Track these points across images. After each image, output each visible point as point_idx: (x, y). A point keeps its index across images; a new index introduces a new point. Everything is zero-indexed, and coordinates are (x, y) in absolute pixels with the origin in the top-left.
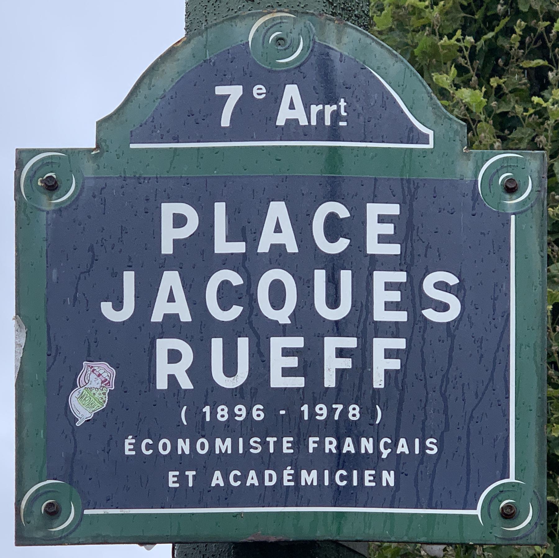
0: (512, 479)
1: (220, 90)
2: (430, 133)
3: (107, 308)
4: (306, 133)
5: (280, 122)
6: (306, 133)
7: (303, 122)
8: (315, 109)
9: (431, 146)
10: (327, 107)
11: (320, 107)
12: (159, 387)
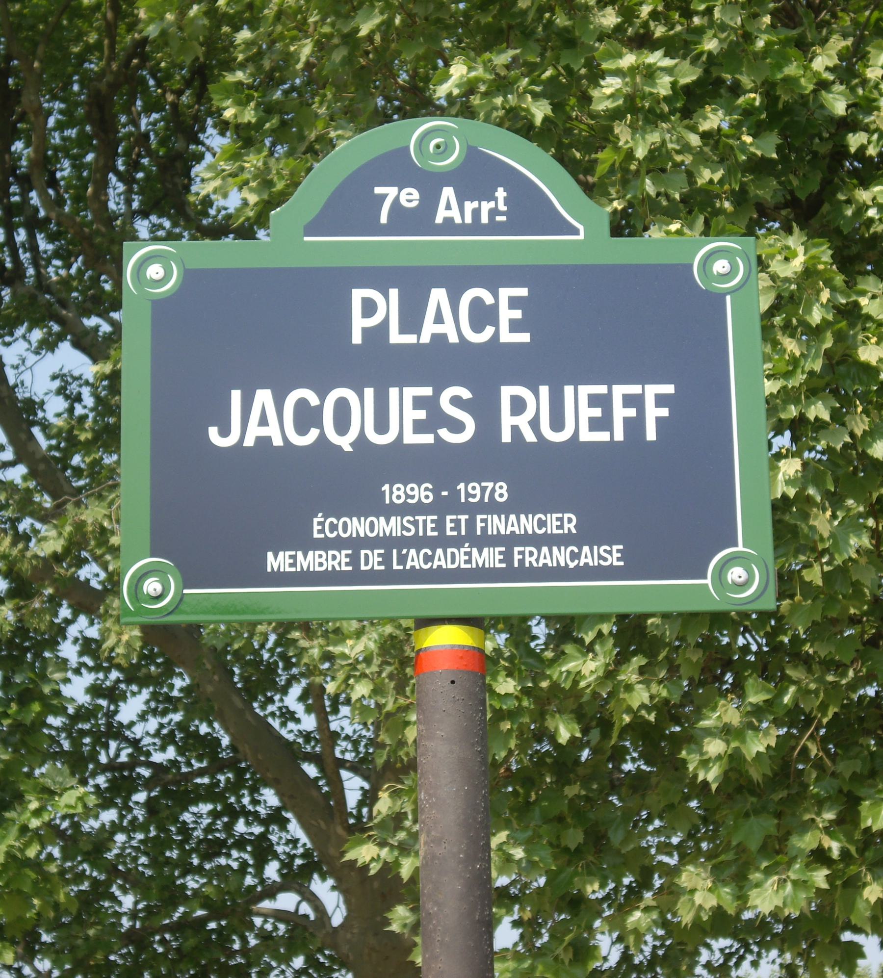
0: (740, 548)
1: (378, 190)
2: (581, 228)
3: (213, 432)
4: (463, 229)
5: (439, 220)
6: (463, 229)
7: (458, 220)
8: (469, 206)
9: (581, 237)
10: (484, 203)
11: (475, 204)
12: (673, 391)
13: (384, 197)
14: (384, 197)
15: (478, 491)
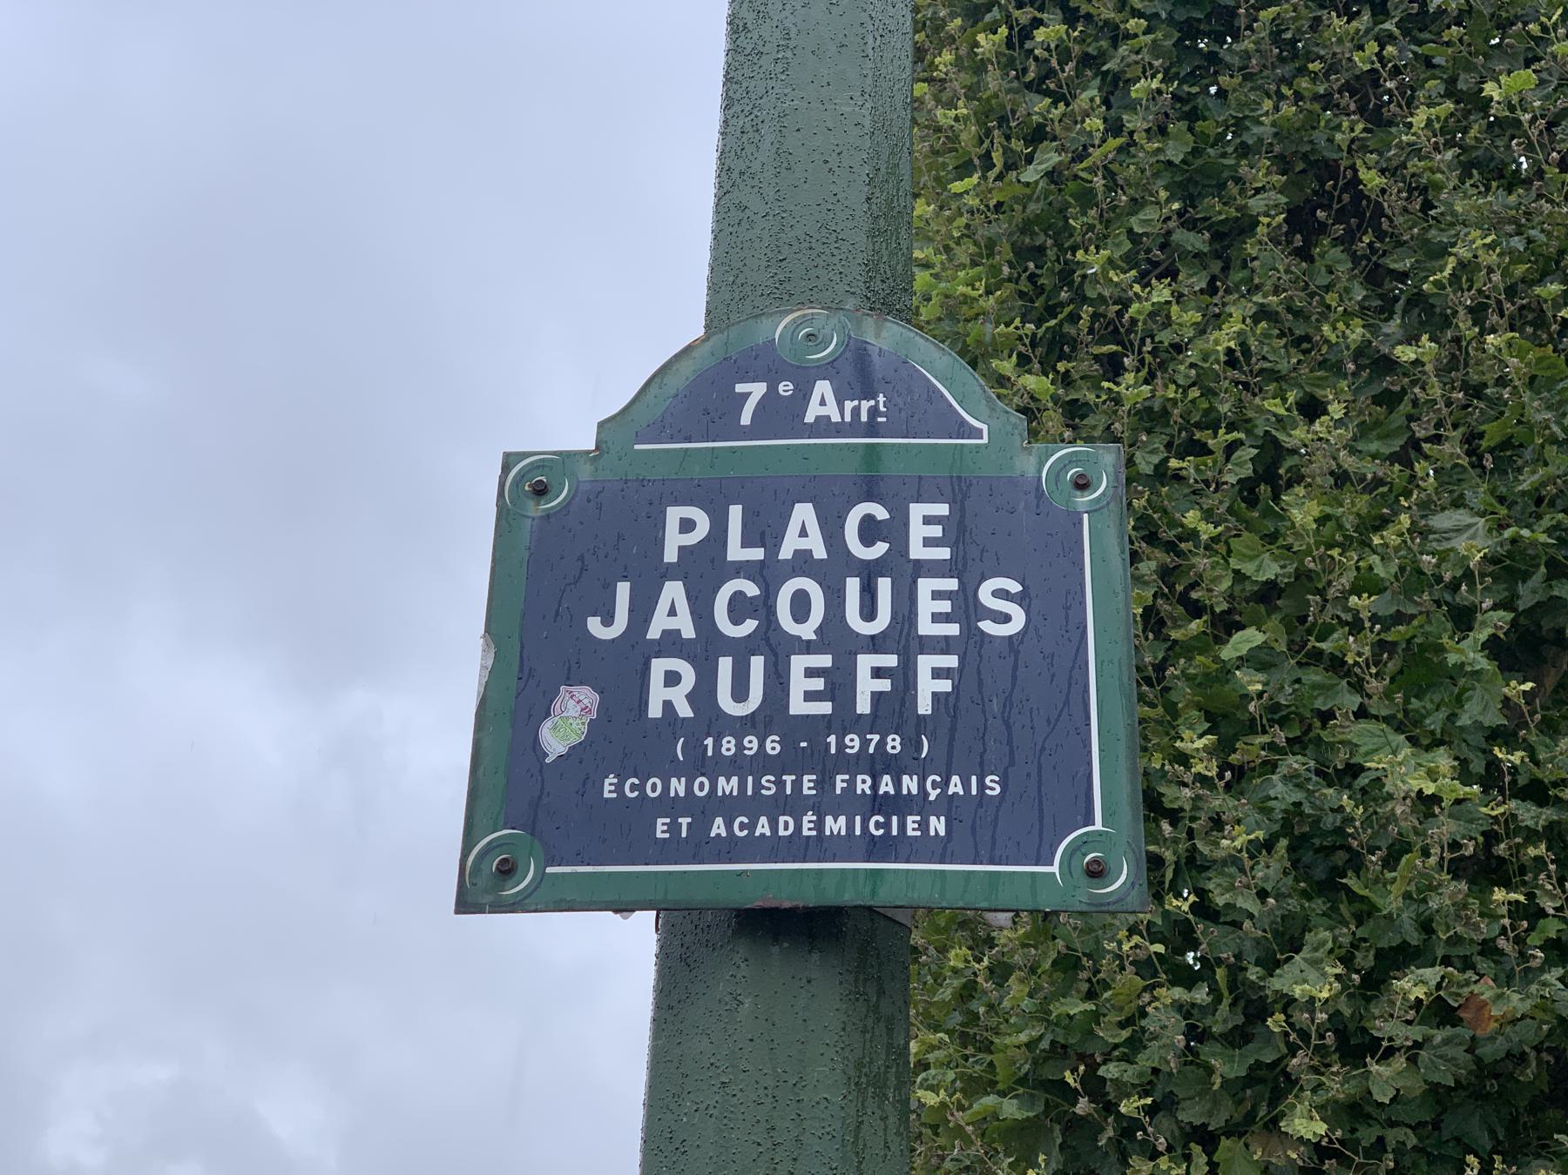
3: (594, 625)
5: (809, 418)
9: (985, 440)
10: (864, 403)
11: (856, 403)
13: (747, 395)
14: (747, 395)
15: (857, 743)
